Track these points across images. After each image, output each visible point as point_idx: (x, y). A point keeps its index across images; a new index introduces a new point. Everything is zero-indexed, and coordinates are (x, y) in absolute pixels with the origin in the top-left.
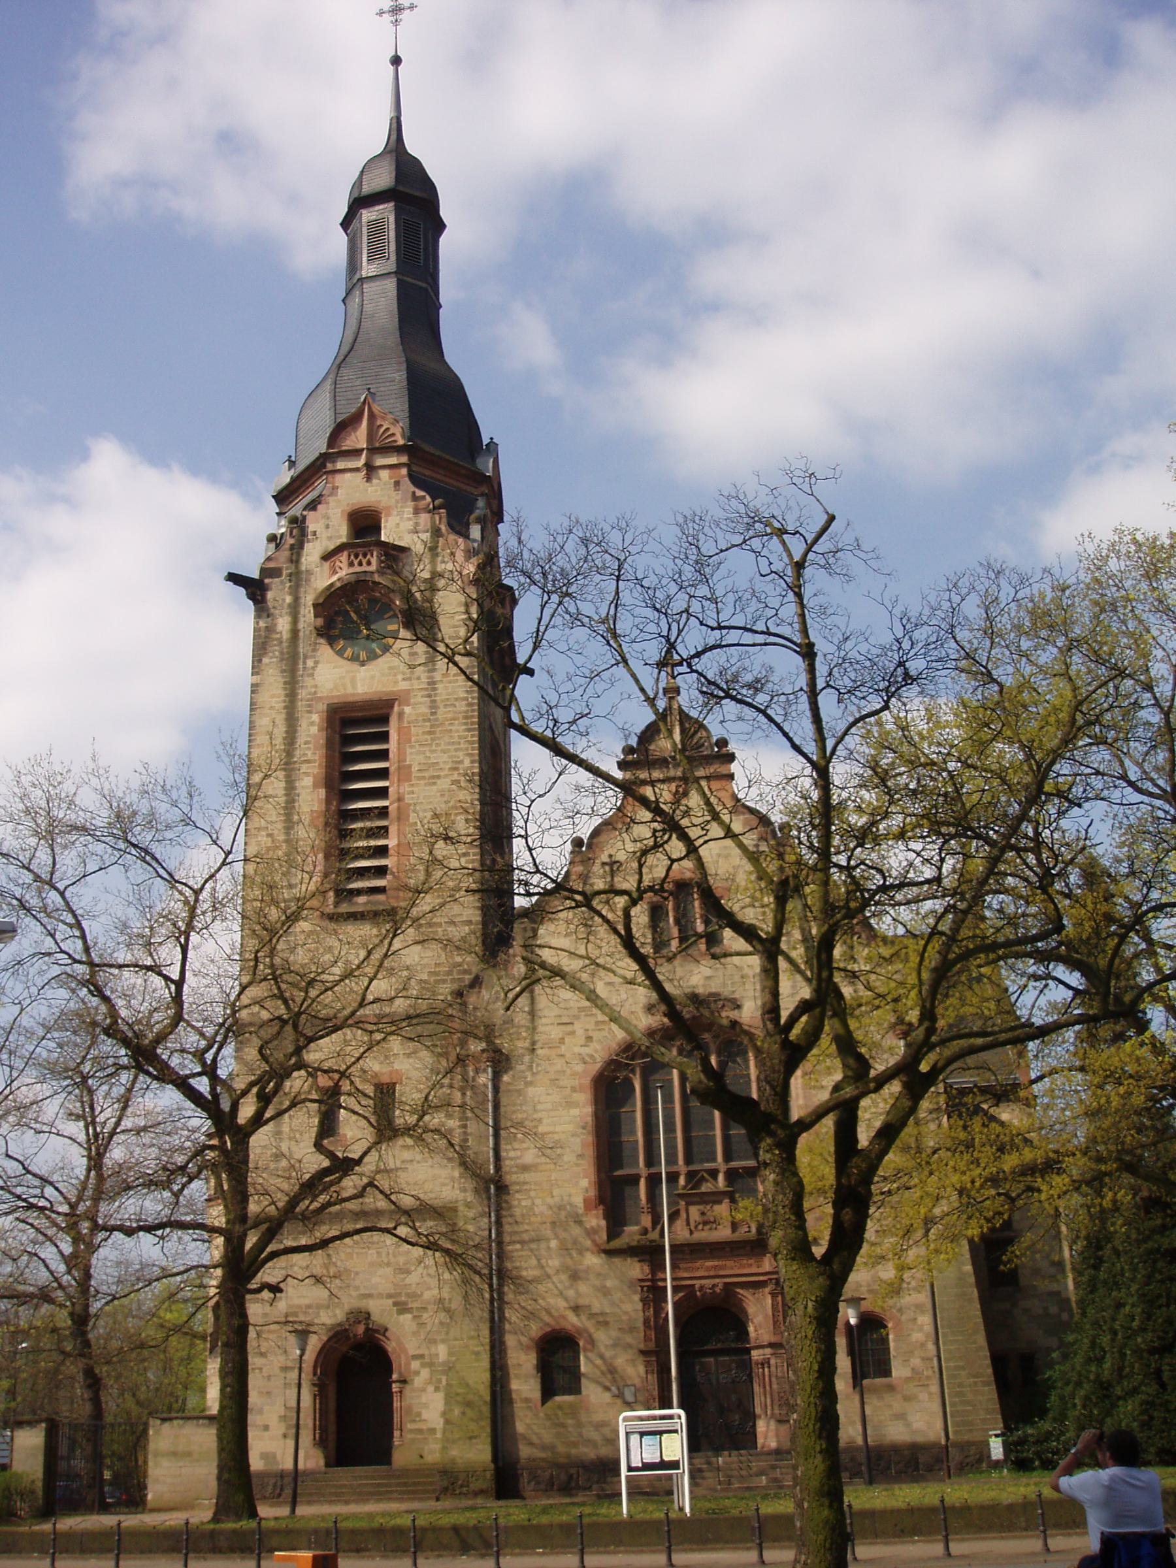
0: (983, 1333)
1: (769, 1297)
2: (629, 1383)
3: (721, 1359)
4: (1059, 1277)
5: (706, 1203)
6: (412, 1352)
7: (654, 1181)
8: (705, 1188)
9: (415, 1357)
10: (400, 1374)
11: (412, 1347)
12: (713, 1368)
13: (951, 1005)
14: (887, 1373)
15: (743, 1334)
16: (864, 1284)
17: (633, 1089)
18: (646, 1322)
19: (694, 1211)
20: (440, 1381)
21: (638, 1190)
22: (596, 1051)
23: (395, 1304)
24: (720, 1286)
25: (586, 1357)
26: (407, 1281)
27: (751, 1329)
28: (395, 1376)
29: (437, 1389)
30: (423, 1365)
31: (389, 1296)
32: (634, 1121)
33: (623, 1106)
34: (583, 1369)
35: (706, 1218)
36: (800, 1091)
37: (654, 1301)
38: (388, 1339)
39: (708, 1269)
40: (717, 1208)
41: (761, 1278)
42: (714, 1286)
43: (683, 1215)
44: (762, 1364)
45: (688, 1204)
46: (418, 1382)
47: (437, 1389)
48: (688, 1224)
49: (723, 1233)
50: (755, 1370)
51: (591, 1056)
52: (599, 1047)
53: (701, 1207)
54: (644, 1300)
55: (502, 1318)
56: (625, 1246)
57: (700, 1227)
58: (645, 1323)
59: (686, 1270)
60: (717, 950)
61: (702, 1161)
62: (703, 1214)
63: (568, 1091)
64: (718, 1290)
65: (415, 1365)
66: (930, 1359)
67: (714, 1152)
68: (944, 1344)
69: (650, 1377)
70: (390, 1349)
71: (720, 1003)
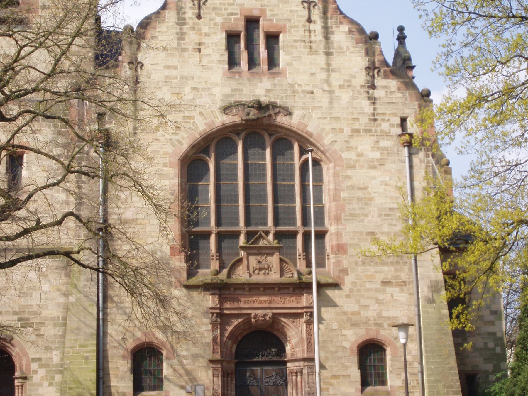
0: (455, 357)
1: (305, 324)
2: (200, 383)
3: (265, 368)
4: (497, 322)
5: (262, 254)
6: (32, 356)
7: (307, 236)
8: (262, 243)
9: (34, 360)
10: (22, 372)
11: (32, 353)
12: (259, 374)
13: (116, 38)
14: (383, 382)
15: (282, 350)
16: (372, 319)
17: (208, 169)
18: (214, 340)
19: (253, 260)
20: (53, 378)
21: (209, 243)
22: (183, 138)
23: (20, 320)
24: (270, 315)
25: (168, 364)
26: (30, 303)
27: (288, 348)
28: (17, 374)
29: (51, 384)
30: (41, 366)
31: (15, 313)
32: (208, 192)
33: (200, 181)
34: (165, 372)
35: (261, 266)
36: (331, 178)
37: (221, 324)
38: (12, 345)
39: (261, 302)
40: (269, 258)
41: (300, 311)
42: (265, 315)
43: (245, 262)
44: (296, 373)
45: (249, 255)
46: (36, 379)
47: (51, 384)
48: (248, 269)
49: (274, 277)
50: (289, 378)
51: (180, 142)
52: (185, 135)
53: (258, 257)
54: (214, 324)
55: (105, 333)
56: (201, 283)
57: (257, 272)
58: (213, 340)
59: (246, 303)
60: (274, 70)
61: (257, 224)
62: (259, 262)
63: (161, 166)
64: (268, 319)
65: (34, 366)
66: (416, 374)
67: (266, 219)
68: (427, 363)
69: (215, 379)
70: (13, 354)
71: (277, 110)
